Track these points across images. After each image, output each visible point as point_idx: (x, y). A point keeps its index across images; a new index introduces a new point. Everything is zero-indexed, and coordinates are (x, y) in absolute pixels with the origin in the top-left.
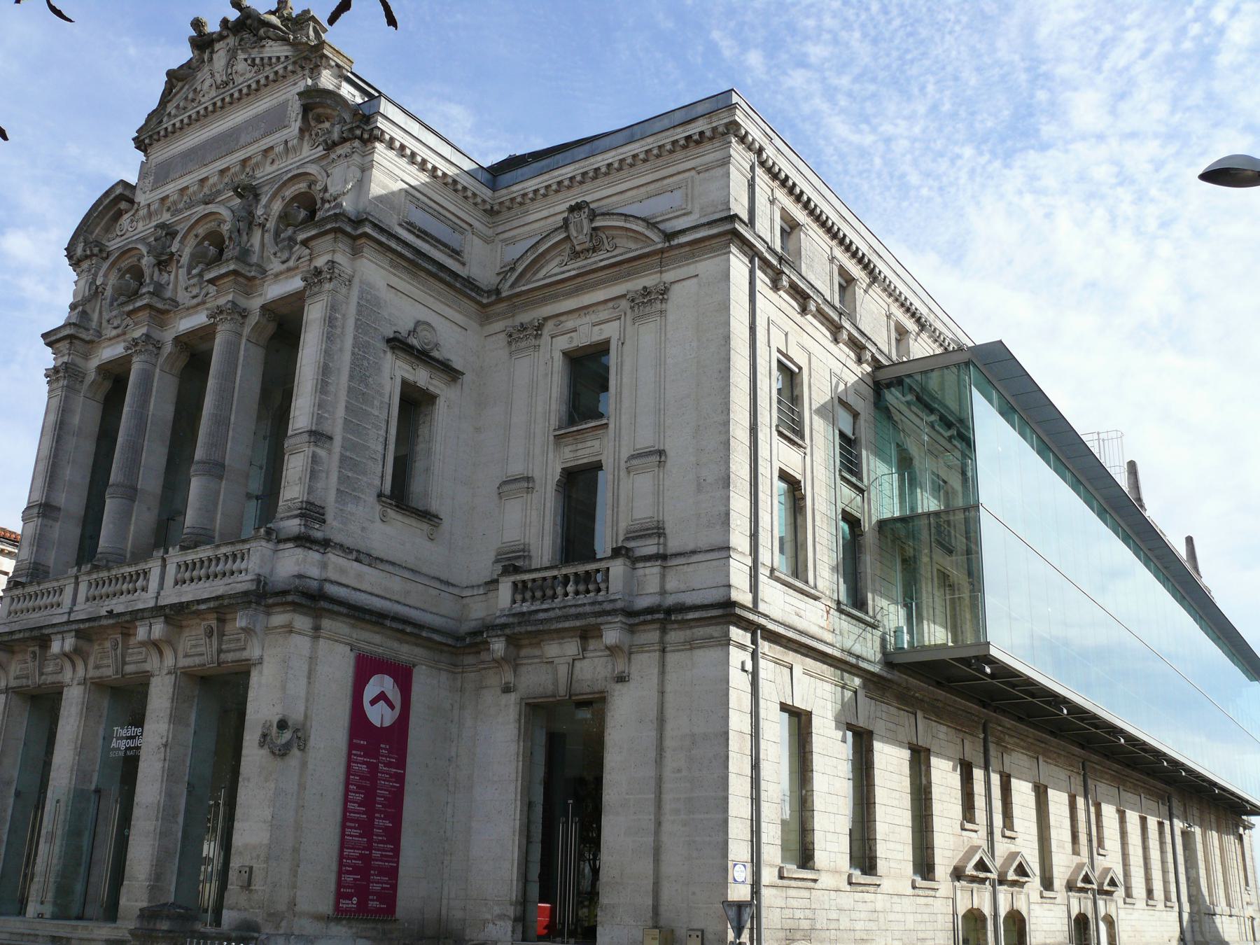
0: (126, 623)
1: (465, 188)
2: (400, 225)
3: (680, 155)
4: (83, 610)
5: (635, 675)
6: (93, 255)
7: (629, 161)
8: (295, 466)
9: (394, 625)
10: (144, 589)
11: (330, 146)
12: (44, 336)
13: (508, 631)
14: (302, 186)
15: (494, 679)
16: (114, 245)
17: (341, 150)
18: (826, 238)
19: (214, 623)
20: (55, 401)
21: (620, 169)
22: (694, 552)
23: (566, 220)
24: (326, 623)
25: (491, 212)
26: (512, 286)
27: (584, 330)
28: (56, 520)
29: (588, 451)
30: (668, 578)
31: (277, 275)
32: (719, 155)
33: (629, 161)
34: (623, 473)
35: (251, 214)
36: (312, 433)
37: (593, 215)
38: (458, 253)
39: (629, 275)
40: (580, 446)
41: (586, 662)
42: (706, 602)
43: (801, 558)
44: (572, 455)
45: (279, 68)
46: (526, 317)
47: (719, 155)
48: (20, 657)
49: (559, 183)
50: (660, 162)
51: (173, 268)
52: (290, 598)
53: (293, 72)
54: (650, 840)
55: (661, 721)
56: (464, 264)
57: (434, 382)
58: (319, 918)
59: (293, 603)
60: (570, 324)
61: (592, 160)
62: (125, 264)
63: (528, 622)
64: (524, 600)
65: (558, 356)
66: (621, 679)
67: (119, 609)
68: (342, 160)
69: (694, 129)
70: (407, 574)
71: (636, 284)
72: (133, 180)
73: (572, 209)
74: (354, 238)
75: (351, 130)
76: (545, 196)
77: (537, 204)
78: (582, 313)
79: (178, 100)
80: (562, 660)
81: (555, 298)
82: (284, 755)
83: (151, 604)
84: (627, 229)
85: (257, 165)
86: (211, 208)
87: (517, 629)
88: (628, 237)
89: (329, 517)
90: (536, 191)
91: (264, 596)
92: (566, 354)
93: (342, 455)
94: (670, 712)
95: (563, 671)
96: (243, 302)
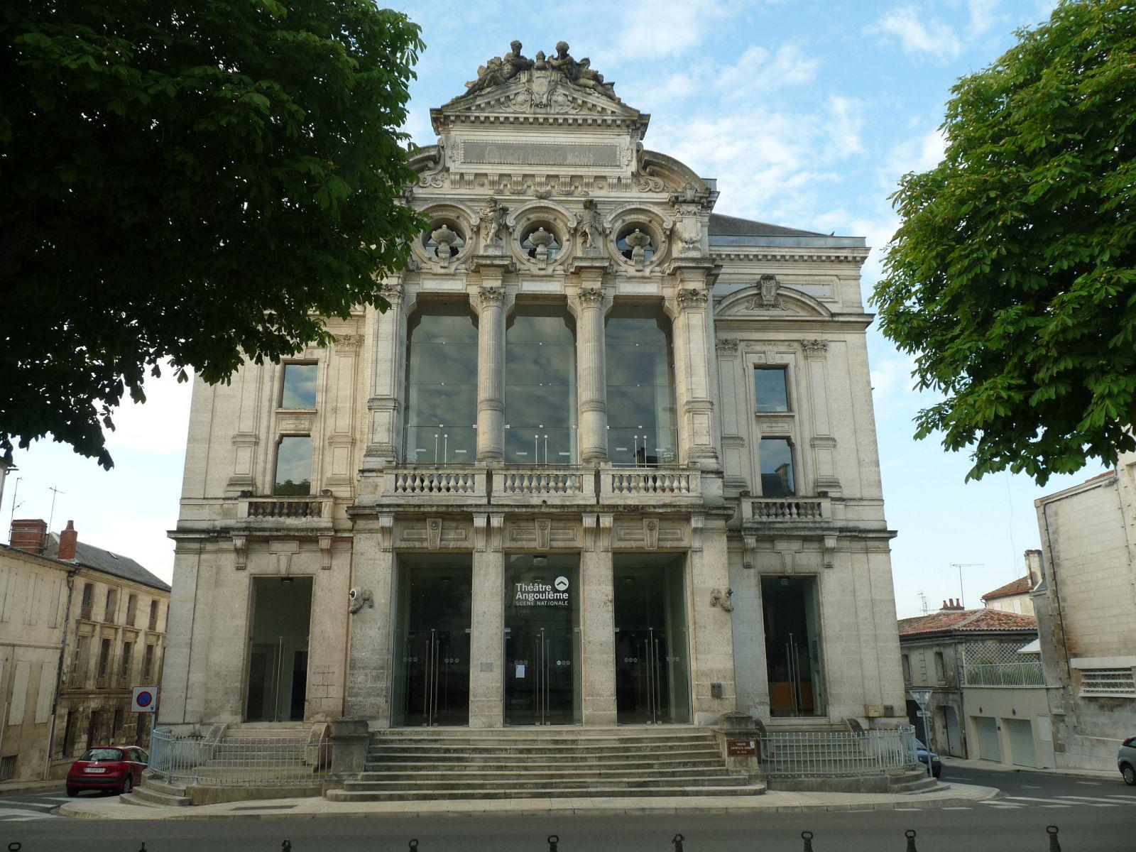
13: (760, 533)
29: (780, 429)
32: (853, 273)
37: (779, 286)
39: (800, 329)
40: (774, 425)
42: (873, 528)
44: (769, 429)
47: (853, 273)
66: (829, 566)
69: (842, 254)
75: (701, 198)
78: (766, 343)
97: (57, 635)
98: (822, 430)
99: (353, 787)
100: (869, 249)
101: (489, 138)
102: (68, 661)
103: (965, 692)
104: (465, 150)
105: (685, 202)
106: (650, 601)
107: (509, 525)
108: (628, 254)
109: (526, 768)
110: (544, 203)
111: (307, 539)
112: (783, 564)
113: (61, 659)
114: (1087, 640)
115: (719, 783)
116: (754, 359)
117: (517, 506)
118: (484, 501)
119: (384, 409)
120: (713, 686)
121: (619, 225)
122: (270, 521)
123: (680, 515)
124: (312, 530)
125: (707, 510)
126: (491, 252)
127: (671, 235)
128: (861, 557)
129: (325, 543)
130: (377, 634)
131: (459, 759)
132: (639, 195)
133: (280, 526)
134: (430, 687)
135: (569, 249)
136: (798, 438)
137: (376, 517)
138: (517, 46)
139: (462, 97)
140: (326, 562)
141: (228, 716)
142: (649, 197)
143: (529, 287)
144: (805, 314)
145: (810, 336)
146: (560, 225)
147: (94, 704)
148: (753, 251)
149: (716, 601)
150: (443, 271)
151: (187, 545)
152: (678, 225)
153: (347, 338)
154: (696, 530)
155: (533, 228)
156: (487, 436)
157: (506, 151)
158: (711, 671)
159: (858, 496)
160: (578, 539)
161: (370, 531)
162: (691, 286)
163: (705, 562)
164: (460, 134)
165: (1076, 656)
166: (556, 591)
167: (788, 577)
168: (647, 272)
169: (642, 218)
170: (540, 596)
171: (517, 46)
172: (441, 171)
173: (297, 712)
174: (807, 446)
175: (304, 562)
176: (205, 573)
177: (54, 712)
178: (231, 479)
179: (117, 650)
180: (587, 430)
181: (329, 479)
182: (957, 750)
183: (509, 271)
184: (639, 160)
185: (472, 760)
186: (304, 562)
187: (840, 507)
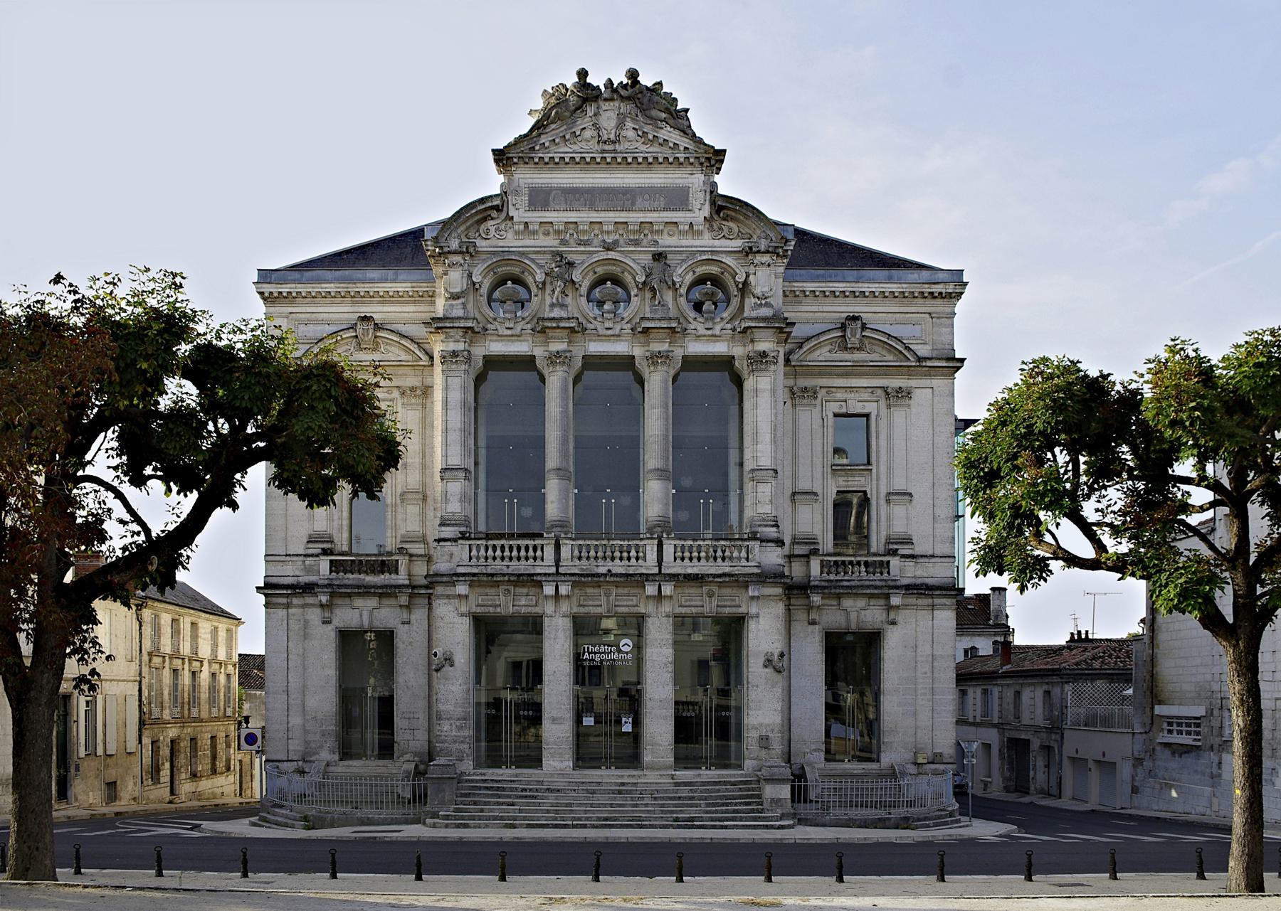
37: (864, 327)
47: (948, 310)
66: (894, 623)
69: (937, 289)
73: (848, 318)
81: (830, 375)
97: (134, 667)
98: (899, 485)
99: (447, 817)
100: (966, 284)
101: (555, 181)
102: (145, 693)
103: (1066, 733)
104: (530, 196)
105: (759, 252)
106: (717, 655)
107: (576, 591)
108: (698, 307)
109: (591, 805)
110: (612, 255)
111: (386, 593)
112: (848, 620)
113: (140, 690)
114: (1170, 687)
115: (755, 819)
116: (834, 407)
117: (582, 575)
118: (553, 570)
119: (455, 479)
120: (761, 738)
121: (689, 278)
122: (352, 578)
123: (740, 582)
124: (391, 586)
125: (765, 577)
126: (557, 313)
127: (745, 288)
128: (924, 615)
129: (403, 599)
130: (456, 690)
131: (533, 797)
132: (711, 242)
133: (360, 583)
134: (507, 725)
135: (638, 306)
136: (874, 492)
137: (453, 584)
138: (583, 74)
139: (526, 135)
140: (405, 616)
141: (326, 754)
142: (726, 245)
143: (596, 348)
144: (891, 358)
145: (894, 383)
146: (628, 278)
147: (172, 732)
148: (840, 287)
149: (768, 663)
150: (509, 332)
151: (275, 600)
152: (752, 278)
153: (413, 389)
154: (753, 598)
155: (600, 282)
156: (555, 505)
157: (574, 197)
158: (761, 725)
159: (930, 552)
160: (642, 605)
161: (448, 597)
162: (762, 346)
163: (760, 627)
164: (527, 177)
165: (1160, 703)
166: (619, 651)
167: (853, 633)
168: (717, 331)
169: (714, 269)
170: (605, 657)
171: (583, 74)
172: (505, 220)
173: (386, 750)
174: (882, 502)
175: (386, 615)
176: (295, 626)
177: (140, 742)
178: (310, 536)
179: (186, 679)
180: (655, 499)
181: (403, 536)
182: (1054, 791)
183: (577, 331)
184: (713, 203)
185: (547, 798)
186: (386, 615)
187: (910, 564)
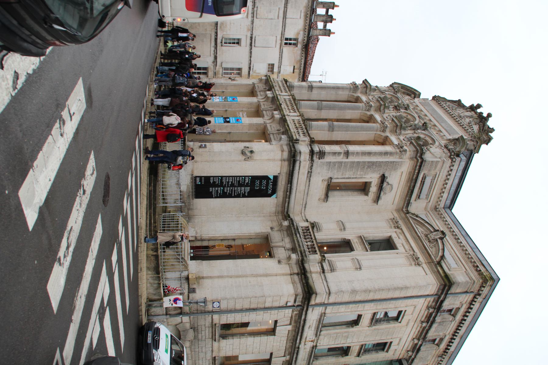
0: (279, 108)
1: (442, 197)
2: (424, 174)
3: (471, 265)
4: (281, 99)
5: (281, 266)
6: (395, 89)
7: (464, 249)
8: (336, 148)
9: (289, 188)
10: (290, 112)
11: (446, 147)
12: (366, 80)
13: (291, 225)
14: (430, 141)
15: (275, 224)
16: (399, 95)
17: (445, 150)
18: (452, 332)
19: (282, 131)
20: (346, 86)
21: (460, 246)
22: (327, 281)
23: (438, 230)
24: (286, 163)
25: (436, 208)
26: (411, 217)
27: (400, 241)
28: (308, 91)
30: (317, 274)
31: (399, 138)
33: (464, 249)
34: (351, 258)
35: (418, 129)
36: (348, 151)
37: (441, 239)
38: (419, 198)
41: (284, 251)
43: (330, 328)
45: (470, 130)
46: (401, 223)
48: (264, 86)
49: (451, 228)
50: (466, 259)
51: (395, 111)
52: (293, 149)
53: (469, 135)
54: (226, 274)
55: (266, 275)
56: (415, 200)
57: (373, 194)
58: (192, 171)
59: (291, 150)
60: (401, 237)
61: (462, 237)
62: (394, 99)
63: (295, 231)
64: (303, 230)
65: (389, 234)
66: (279, 262)
67: (283, 106)
68: (442, 151)
70: (306, 191)
71: (419, 254)
72: (421, 97)
74: (416, 158)
75: (453, 151)
76: (445, 224)
77: (442, 222)
79: (451, 105)
80: (284, 244)
81: (410, 231)
82: (242, 153)
83: (285, 114)
84: (439, 251)
85: (435, 129)
86: (417, 118)
87: (292, 228)
88: (436, 251)
89: (321, 160)
90: (446, 221)
91: (293, 142)
92: (390, 237)
93: (342, 162)
94: (270, 278)
95: (281, 244)
96: (388, 130)
